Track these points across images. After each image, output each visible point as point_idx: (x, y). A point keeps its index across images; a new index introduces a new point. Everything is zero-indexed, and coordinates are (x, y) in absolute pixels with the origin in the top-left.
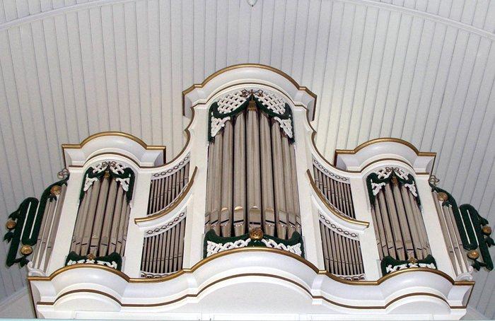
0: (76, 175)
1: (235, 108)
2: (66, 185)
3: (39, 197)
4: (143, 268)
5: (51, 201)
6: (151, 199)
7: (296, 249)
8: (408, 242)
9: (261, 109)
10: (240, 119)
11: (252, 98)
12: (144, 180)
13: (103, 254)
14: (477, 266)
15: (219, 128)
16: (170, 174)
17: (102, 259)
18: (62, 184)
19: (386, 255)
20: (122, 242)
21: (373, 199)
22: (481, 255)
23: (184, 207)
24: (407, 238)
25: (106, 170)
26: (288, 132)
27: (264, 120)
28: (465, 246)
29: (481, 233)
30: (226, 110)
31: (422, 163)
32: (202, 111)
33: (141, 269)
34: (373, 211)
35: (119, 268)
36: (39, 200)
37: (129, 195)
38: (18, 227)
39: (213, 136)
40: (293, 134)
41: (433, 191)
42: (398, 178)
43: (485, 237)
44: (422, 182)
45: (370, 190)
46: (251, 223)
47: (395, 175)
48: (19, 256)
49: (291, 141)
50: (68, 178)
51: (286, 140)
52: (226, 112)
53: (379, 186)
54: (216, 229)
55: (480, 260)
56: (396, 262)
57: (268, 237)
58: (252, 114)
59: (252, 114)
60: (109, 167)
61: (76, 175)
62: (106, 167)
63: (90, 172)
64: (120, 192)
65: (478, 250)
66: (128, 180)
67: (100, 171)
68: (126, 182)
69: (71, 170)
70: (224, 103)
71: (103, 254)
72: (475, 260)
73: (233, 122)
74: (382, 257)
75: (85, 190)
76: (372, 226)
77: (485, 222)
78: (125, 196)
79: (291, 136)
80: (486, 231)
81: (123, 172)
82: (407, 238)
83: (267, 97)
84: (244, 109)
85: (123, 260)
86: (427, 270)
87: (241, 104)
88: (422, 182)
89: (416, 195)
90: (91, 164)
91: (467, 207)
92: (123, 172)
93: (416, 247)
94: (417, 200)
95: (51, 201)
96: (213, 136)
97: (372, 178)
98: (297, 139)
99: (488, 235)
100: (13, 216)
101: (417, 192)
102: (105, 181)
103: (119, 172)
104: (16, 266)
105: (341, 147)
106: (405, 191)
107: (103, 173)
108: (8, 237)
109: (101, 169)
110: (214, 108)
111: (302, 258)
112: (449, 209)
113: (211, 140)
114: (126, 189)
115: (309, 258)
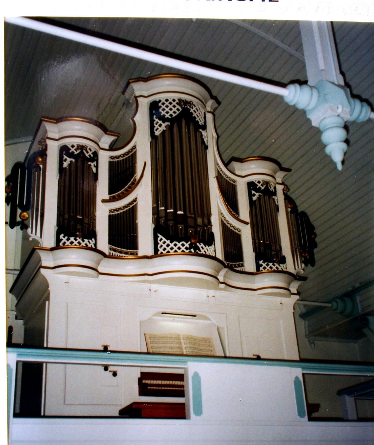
1: (174, 115)
23: (136, 194)
31: (280, 176)
52: (167, 116)
68: (94, 165)
70: (163, 107)
81: (92, 155)
87: (178, 112)
90: (68, 142)
92: (92, 155)
103: (90, 155)
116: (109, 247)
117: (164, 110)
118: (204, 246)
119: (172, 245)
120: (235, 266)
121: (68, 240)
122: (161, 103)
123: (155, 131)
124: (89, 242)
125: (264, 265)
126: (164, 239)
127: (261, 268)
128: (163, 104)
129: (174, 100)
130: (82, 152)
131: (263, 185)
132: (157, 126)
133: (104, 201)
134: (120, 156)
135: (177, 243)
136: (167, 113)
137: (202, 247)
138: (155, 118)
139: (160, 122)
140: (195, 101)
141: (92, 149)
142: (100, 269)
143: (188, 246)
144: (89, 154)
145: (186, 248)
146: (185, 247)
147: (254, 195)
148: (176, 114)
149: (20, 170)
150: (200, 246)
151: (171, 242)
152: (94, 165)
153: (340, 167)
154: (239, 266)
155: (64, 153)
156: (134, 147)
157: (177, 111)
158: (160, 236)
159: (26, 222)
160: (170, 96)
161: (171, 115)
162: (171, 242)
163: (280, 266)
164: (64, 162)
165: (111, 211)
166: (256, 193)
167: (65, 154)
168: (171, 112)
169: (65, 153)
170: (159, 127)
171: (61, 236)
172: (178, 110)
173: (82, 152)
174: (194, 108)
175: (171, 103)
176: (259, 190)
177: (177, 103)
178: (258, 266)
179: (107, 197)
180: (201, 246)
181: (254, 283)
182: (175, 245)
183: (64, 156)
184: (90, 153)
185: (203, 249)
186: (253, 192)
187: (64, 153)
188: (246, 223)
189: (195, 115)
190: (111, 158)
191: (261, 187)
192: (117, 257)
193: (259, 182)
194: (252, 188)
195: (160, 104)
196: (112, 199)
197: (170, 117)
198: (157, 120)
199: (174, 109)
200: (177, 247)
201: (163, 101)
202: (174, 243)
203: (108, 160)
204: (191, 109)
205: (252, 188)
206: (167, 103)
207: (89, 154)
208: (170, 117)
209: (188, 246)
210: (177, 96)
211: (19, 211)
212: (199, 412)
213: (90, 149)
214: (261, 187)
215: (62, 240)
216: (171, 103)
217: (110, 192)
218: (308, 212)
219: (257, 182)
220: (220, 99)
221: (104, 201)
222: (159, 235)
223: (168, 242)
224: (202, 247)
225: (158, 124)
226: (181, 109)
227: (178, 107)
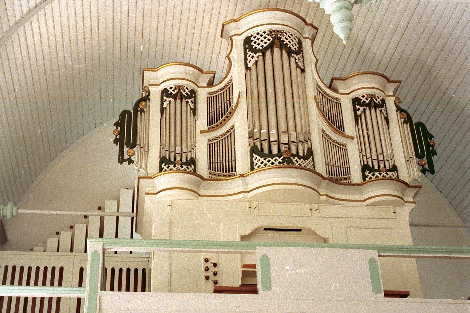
0: (155, 93)
1: (265, 45)
2: (149, 100)
3: (131, 108)
4: (210, 168)
5: (141, 114)
6: (208, 113)
7: (307, 163)
8: (380, 154)
9: (282, 46)
10: (268, 53)
11: (276, 38)
12: (202, 95)
13: (184, 160)
14: (423, 171)
15: (253, 60)
16: (219, 93)
17: (185, 164)
18: (146, 99)
19: (366, 163)
20: (194, 148)
21: (357, 118)
22: (427, 164)
23: (232, 122)
24: (379, 151)
25: (178, 92)
26: (300, 65)
27: (285, 54)
28: (417, 155)
29: (428, 149)
30: (257, 46)
31: (391, 88)
32: (239, 41)
33: (208, 169)
34: (357, 126)
35: (195, 170)
36: (132, 111)
37: (194, 112)
38: (121, 133)
39: (249, 66)
40: (304, 66)
41: (397, 111)
42: (375, 103)
43: (431, 148)
44: (391, 103)
45: (355, 110)
46: (283, 144)
47: (374, 101)
48: (126, 157)
49: (303, 71)
50: (149, 95)
51: (299, 70)
52: (259, 47)
53: (362, 108)
54: (258, 144)
55: (426, 167)
56: (372, 170)
57: (293, 156)
58: (277, 51)
59: (277, 51)
60: (179, 89)
61: (155, 93)
62: (177, 90)
63: (165, 92)
64: (189, 108)
65: (425, 158)
66: (193, 99)
67: (174, 93)
68: (192, 101)
69: (151, 88)
70: (255, 40)
71: (184, 160)
72: (423, 166)
73: (264, 55)
74: (362, 165)
75: (164, 106)
76: (355, 140)
77: (431, 137)
78: (192, 111)
79: (303, 68)
80: (431, 144)
81: (189, 93)
82: (379, 151)
83: (286, 36)
84: (271, 47)
85: (196, 162)
86: (390, 179)
87: (268, 42)
88: (391, 103)
89: (386, 116)
90: (166, 85)
91: (419, 124)
92: (189, 93)
93: (385, 159)
94: (387, 119)
95: (141, 114)
96: (249, 66)
97: (356, 101)
98: (306, 69)
99: (433, 147)
100: (117, 124)
101: (387, 114)
102: (178, 101)
103: (187, 94)
104: (125, 163)
105: (337, 75)
106: (378, 112)
107: (176, 95)
108: (116, 141)
109: (174, 91)
110: (248, 41)
111: (314, 172)
112: (407, 127)
113: (247, 68)
114: (193, 107)
115: (318, 170)
116: (208, 172)
117: (255, 43)
118: (298, 160)
119: (265, 162)
120: (341, 179)
121: (168, 167)
122: (253, 37)
123: (248, 63)
124: (187, 167)
125: (370, 175)
126: (259, 158)
127: (367, 179)
128: (255, 37)
129: (265, 32)
130: (179, 92)
131: (367, 98)
132: (249, 58)
133: (202, 132)
134: (218, 91)
135: (270, 159)
136: (259, 44)
137: (296, 161)
138: (248, 52)
139: (253, 54)
140: (286, 30)
141: (189, 88)
142: (202, 192)
143: (281, 161)
144: (185, 92)
145: (280, 163)
146: (278, 161)
147: (359, 109)
148: (267, 44)
149: (127, 115)
150: (294, 160)
151: (265, 159)
152: (192, 101)
153: (345, 43)
154: (346, 179)
155: (164, 95)
156: (231, 81)
157: (267, 41)
158: (255, 156)
159: (132, 158)
160: (260, 29)
161: (262, 46)
162: (265, 159)
163: (387, 174)
164: (164, 103)
165: (209, 140)
166: (360, 108)
167: (165, 96)
168: (262, 44)
169: (165, 94)
170: (251, 59)
171: (163, 166)
172: (269, 40)
173: (179, 92)
174: (286, 36)
175: (261, 36)
176: (364, 104)
177: (268, 35)
178: (364, 177)
179: (206, 128)
180: (295, 159)
181: (362, 195)
182: (269, 161)
183: (164, 97)
184: (187, 91)
185: (297, 162)
186: (358, 107)
187: (164, 95)
188: (353, 138)
189: (286, 41)
190: (209, 94)
191: (366, 100)
192: (214, 179)
193: (363, 96)
194: (356, 103)
195: (252, 39)
196: (209, 131)
197: (261, 48)
198: (249, 53)
199: (266, 40)
200: (271, 162)
201: (255, 35)
202: (267, 160)
203: (206, 95)
204: (282, 37)
205: (356, 103)
206: (258, 36)
207: (185, 92)
208: (261, 48)
209: (281, 161)
210: (266, 28)
211: (126, 149)
212: (268, 287)
213: (187, 89)
214: (366, 100)
215: (163, 168)
216: (261, 36)
217: (209, 124)
218: (423, 121)
219: (361, 96)
220: (316, 25)
221: (202, 132)
222: (254, 155)
223: (262, 159)
224: (296, 161)
225: (251, 57)
226: (271, 39)
227: (268, 37)
